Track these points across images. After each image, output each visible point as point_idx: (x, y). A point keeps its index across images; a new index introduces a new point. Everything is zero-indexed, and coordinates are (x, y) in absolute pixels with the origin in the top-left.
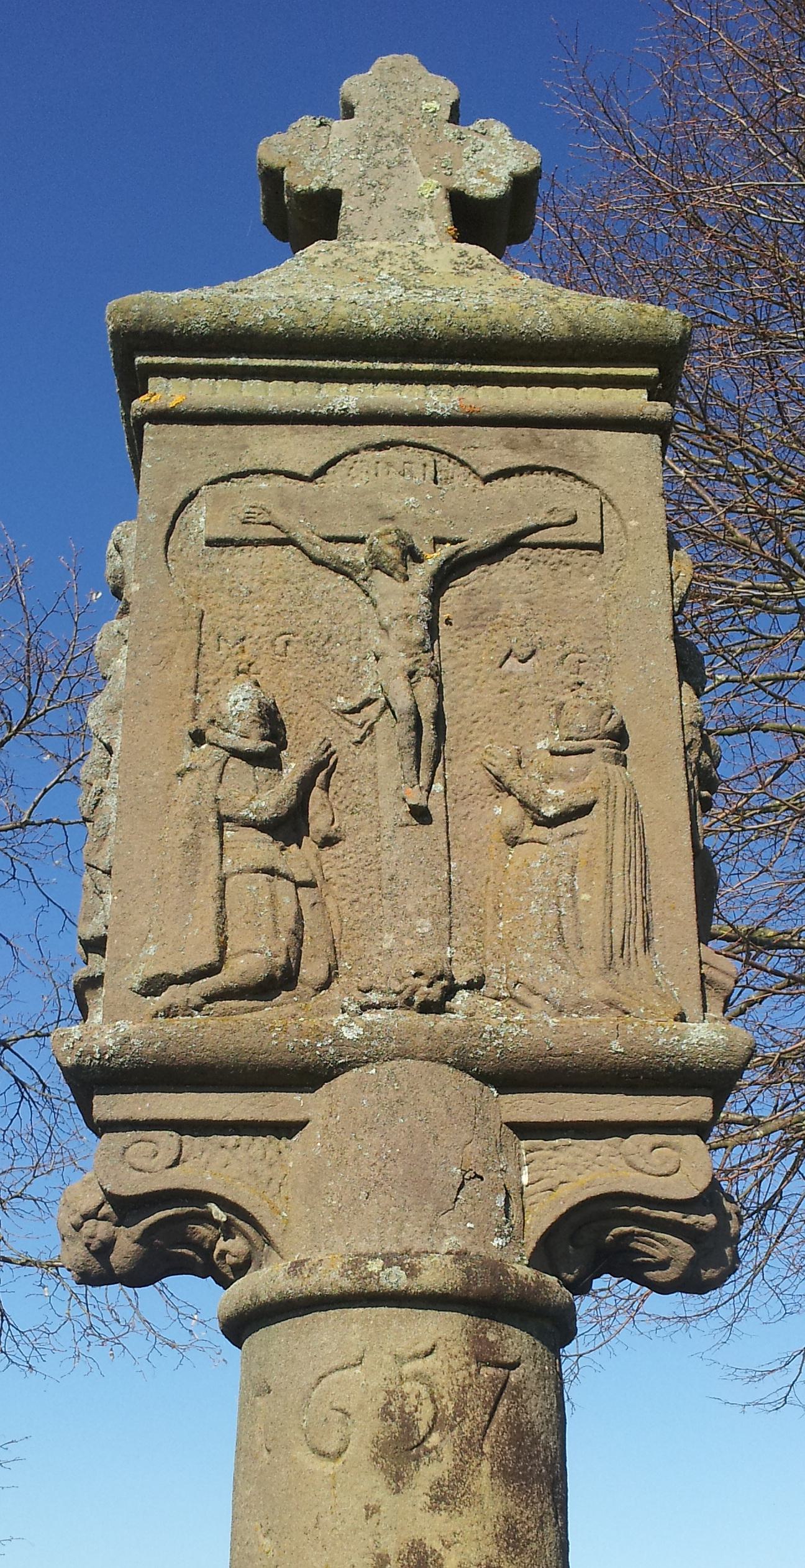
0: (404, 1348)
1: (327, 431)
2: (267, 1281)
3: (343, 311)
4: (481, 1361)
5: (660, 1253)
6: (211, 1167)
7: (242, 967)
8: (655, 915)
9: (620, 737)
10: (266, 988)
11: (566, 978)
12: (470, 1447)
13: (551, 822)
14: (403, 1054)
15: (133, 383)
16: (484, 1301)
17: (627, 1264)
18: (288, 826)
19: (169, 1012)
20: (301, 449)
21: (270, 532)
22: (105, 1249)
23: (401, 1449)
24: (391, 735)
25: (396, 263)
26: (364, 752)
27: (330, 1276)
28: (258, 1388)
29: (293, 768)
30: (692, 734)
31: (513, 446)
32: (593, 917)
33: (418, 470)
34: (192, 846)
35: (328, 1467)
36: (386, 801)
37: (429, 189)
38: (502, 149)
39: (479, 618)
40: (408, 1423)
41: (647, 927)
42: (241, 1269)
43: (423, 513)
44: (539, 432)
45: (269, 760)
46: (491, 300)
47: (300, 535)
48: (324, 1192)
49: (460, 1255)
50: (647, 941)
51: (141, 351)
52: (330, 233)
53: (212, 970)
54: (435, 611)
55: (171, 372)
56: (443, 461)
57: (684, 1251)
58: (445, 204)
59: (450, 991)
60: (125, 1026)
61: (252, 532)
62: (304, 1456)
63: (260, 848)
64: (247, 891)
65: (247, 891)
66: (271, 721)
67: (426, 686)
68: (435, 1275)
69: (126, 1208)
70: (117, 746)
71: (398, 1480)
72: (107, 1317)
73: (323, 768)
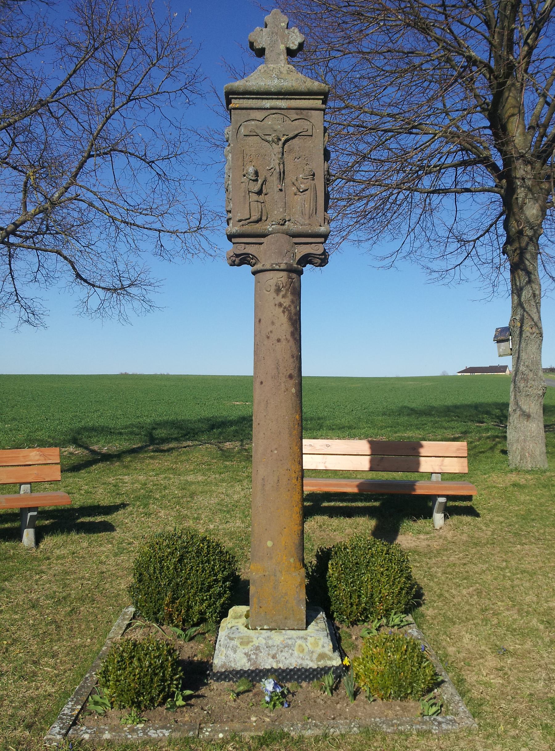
0: (278, 277)
1: (264, 111)
2: (259, 267)
3: (267, 87)
4: (289, 278)
5: (316, 262)
6: (250, 250)
7: (253, 218)
8: (318, 207)
9: (314, 175)
10: (257, 222)
11: (303, 220)
12: (287, 290)
13: (302, 192)
14: (278, 233)
15: (229, 102)
16: (290, 270)
17: (311, 262)
18: (260, 193)
19: (243, 225)
20: (259, 115)
21: (255, 134)
22: (235, 261)
23: (278, 290)
24: (276, 176)
25: (275, 73)
26: (272, 177)
27: (268, 267)
28: (257, 282)
29: (260, 182)
30: (326, 173)
31: (297, 114)
32: (307, 209)
33: (280, 119)
34: (245, 196)
35: (268, 293)
36: (275, 187)
37: (282, 47)
38: (297, 36)
39: (291, 151)
40: (279, 287)
41: (316, 210)
42: (254, 265)
43: (281, 130)
44: (302, 111)
45: (256, 180)
46: (294, 85)
47: (260, 134)
48: (268, 253)
49: (286, 263)
50: (316, 212)
51: (230, 95)
52: (306, 577)
53: (249, 219)
54: (283, 150)
55: (236, 98)
56: (285, 117)
57: (319, 261)
58: (285, 51)
59: (285, 222)
60: (236, 228)
61: (251, 134)
62: (265, 291)
63: (254, 197)
64: (254, 205)
65: (254, 205)
66: (256, 173)
67: (282, 165)
68: (283, 266)
69: (237, 256)
70: (231, 176)
71: (278, 295)
72: (192, 247)
73: (265, 181)
